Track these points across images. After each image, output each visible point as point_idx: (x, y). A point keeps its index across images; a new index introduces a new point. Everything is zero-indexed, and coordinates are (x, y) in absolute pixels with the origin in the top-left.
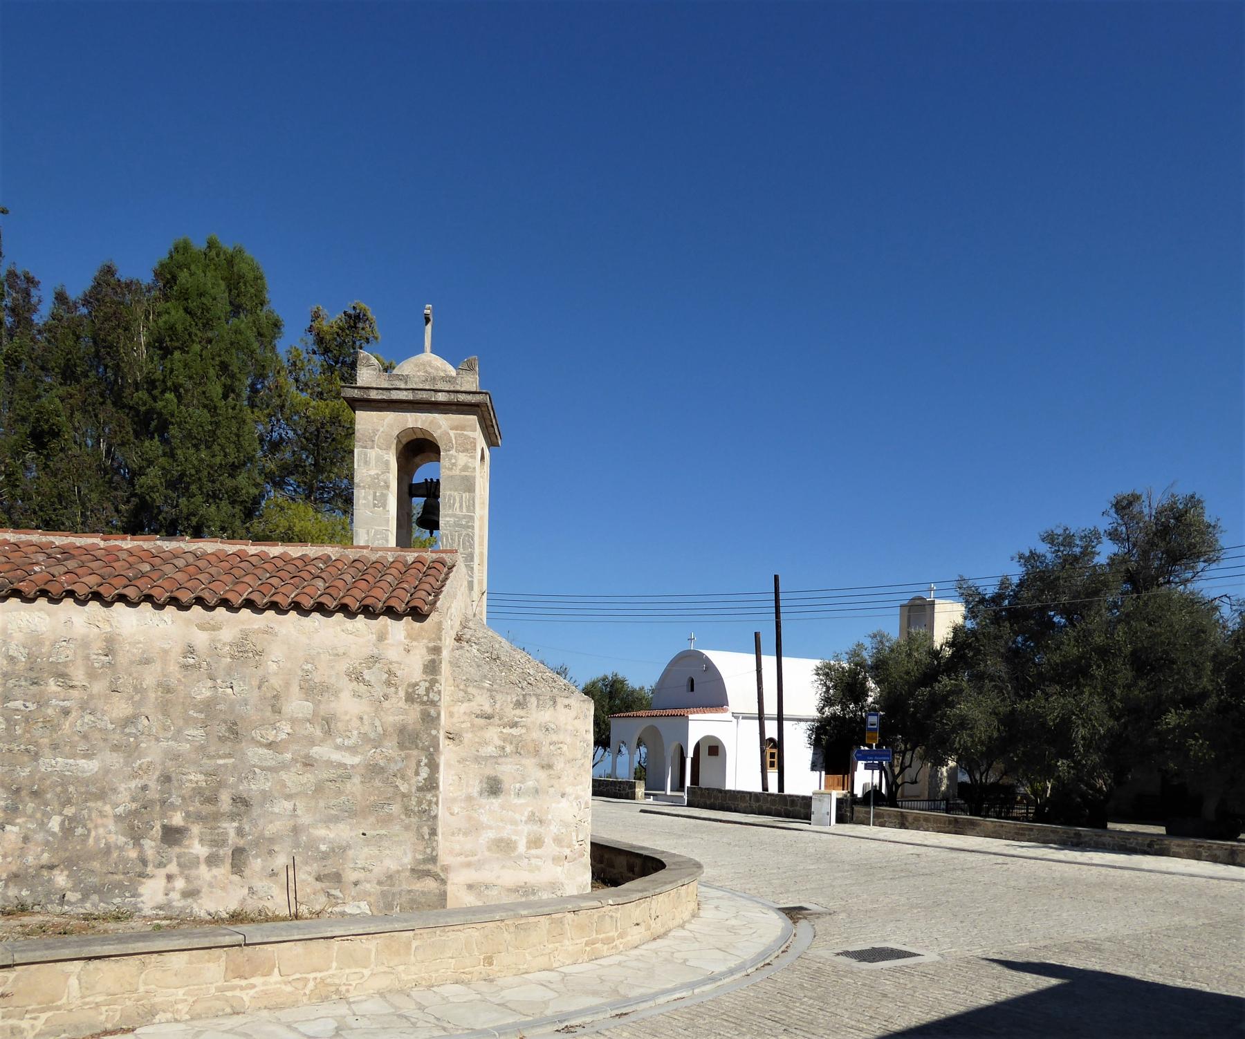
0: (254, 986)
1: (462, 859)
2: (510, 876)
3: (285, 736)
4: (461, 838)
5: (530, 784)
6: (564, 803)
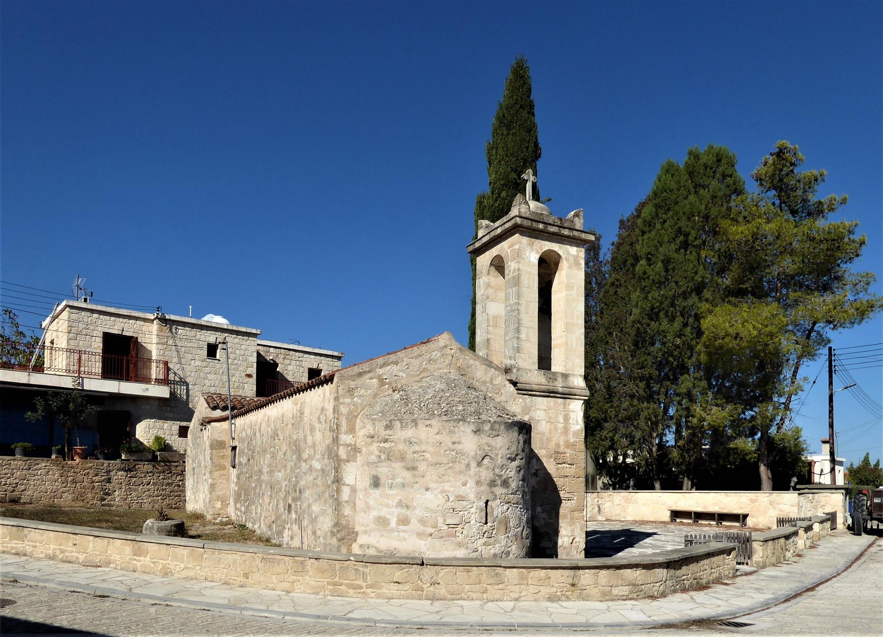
1: (363, 528)
5: (399, 480)
6: (429, 495)
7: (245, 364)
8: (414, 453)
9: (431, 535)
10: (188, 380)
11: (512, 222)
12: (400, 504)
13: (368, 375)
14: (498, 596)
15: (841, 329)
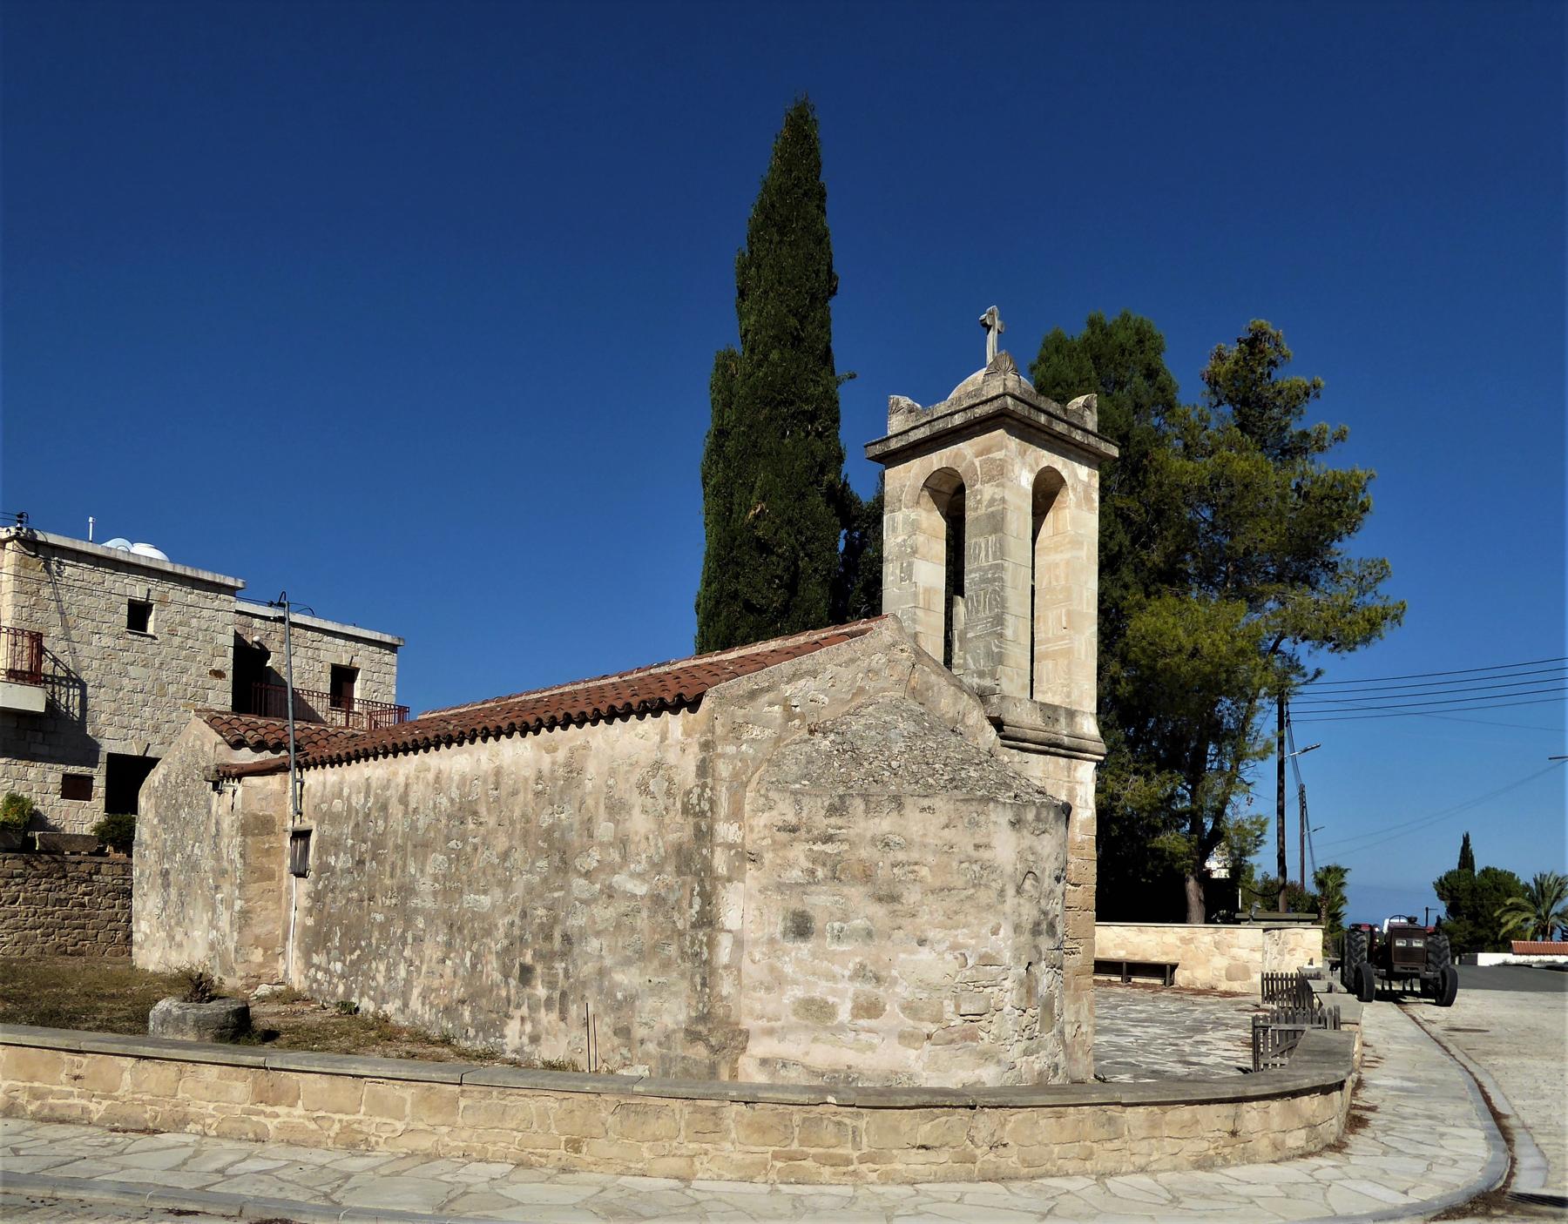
0: (277, 1116)
1: (763, 1023)
2: (824, 1054)
3: (595, 864)
4: (762, 993)
5: (858, 923)
6: (925, 954)
7: (209, 648)
8: (894, 866)
9: (929, 1037)
10: (84, 676)
11: (996, 405)
12: (860, 973)
13: (766, 698)
14: (1111, 1165)
15: (1345, 653)
